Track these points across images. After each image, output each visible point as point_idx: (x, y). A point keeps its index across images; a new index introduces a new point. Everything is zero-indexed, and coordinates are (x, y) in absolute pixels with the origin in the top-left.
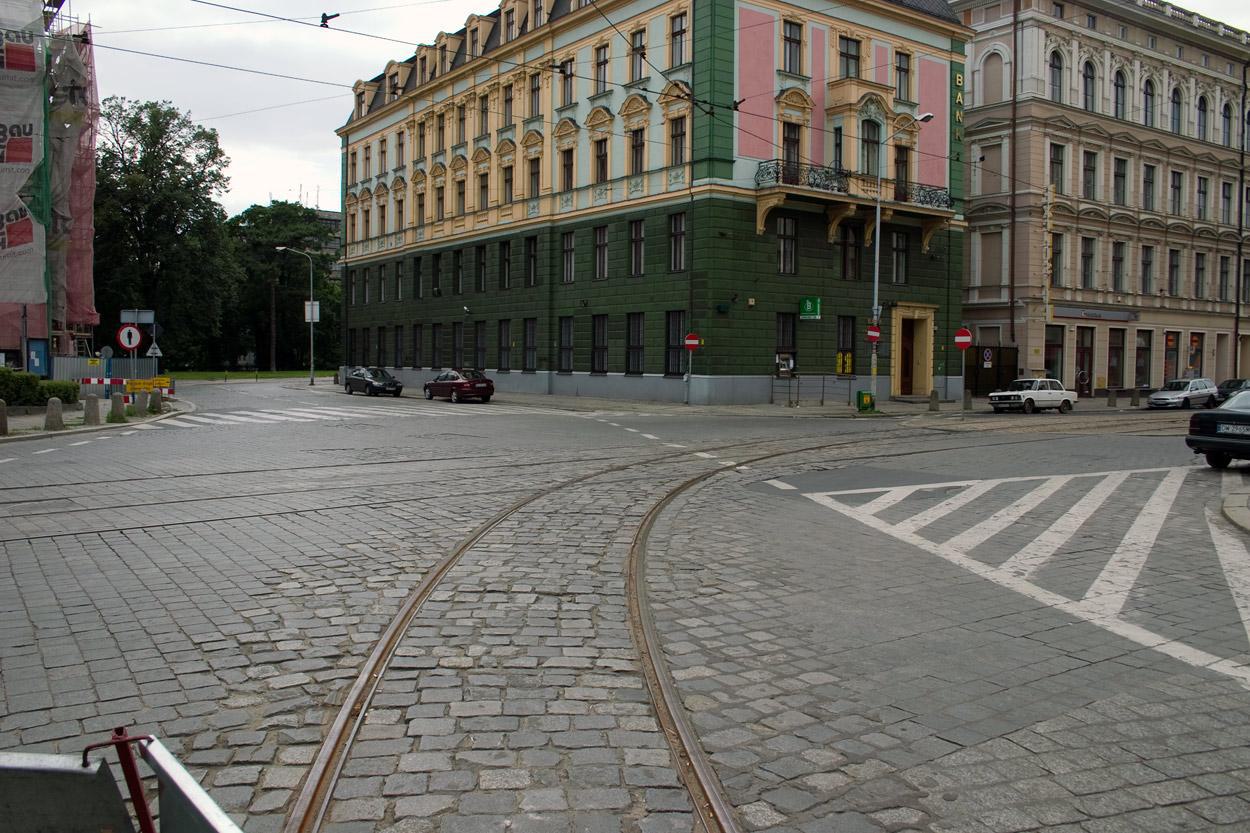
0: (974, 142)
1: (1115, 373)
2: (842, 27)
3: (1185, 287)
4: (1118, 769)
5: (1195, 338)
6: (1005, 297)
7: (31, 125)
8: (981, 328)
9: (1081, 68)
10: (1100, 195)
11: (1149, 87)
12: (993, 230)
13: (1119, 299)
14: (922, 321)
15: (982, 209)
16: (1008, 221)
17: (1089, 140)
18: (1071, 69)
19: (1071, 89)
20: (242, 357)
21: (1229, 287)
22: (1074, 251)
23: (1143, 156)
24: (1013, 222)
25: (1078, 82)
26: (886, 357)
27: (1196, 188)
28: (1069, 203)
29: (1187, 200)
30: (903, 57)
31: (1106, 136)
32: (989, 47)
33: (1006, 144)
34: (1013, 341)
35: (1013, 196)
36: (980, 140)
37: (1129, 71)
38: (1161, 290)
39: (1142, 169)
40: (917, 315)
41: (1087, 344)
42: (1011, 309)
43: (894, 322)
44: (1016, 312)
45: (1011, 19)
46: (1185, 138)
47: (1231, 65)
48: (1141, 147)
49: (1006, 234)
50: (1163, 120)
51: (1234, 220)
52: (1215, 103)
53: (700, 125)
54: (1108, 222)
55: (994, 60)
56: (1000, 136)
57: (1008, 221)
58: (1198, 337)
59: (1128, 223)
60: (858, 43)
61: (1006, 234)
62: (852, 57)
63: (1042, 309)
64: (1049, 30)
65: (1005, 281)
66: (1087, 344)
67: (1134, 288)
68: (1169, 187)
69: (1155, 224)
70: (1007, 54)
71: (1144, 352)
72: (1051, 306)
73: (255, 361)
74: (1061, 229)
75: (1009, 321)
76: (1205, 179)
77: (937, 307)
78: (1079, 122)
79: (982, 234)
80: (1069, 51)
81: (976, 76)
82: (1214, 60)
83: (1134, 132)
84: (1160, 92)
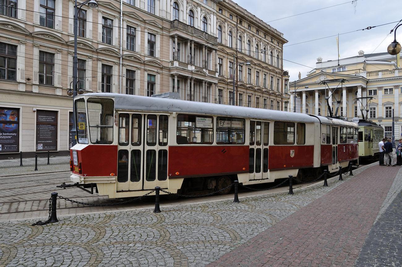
4: (361, 171)
5: (43, 118)
9: (202, 19)
18: (211, 25)
19: (159, 10)
23: (100, 11)
26: (43, 123)
27: (248, 72)
28: (159, 61)
29: (244, 76)
31: (226, 53)
39: (101, 21)
46: (274, 67)
48: (145, 23)
51: (280, 90)
52: (211, 21)
59: (157, 65)
64: (203, 8)
68: (228, 67)
73: (259, 125)
74: (242, 92)
76: (258, 72)
78: (256, 62)
80: (244, 36)
83: (275, 69)
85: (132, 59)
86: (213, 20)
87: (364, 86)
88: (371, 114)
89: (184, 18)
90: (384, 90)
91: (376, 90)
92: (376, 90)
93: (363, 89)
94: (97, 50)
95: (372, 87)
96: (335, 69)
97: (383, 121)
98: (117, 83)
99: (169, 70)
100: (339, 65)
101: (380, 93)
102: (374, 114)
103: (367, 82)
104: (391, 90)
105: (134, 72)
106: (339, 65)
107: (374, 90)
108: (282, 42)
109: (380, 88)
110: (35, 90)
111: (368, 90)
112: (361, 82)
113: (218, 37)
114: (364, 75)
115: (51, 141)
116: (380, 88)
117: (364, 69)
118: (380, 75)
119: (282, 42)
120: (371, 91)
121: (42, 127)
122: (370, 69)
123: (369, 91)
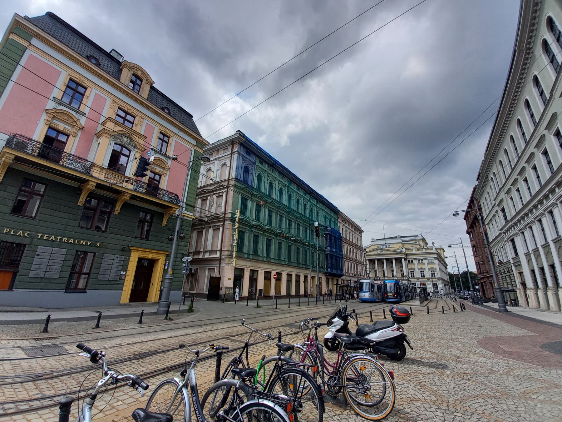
0: (214, 194)
2: (162, 129)
7: (119, 108)
10: (273, 225)
11: (298, 202)
20: (261, 96)
24: (224, 224)
25: (278, 193)
32: (223, 162)
33: (225, 194)
35: (225, 214)
42: (220, 260)
49: (221, 229)
53: (209, 361)
55: (225, 166)
60: (169, 137)
61: (221, 229)
62: (166, 142)
65: (219, 248)
67: (249, 251)
70: (228, 164)
71: (298, 282)
86: (321, 214)
93: (405, 259)
95: (410, 258)
99: (325, 251)
101: (415, 262)
103: (406, 255)
104: (422, 260)
108: (363, 232)
109: (415, 259)
114: (404, 250)
116: (415, 259)
117: (403, 246)
118: (414, 251)
119: (363, 232)
122: (407, 246)
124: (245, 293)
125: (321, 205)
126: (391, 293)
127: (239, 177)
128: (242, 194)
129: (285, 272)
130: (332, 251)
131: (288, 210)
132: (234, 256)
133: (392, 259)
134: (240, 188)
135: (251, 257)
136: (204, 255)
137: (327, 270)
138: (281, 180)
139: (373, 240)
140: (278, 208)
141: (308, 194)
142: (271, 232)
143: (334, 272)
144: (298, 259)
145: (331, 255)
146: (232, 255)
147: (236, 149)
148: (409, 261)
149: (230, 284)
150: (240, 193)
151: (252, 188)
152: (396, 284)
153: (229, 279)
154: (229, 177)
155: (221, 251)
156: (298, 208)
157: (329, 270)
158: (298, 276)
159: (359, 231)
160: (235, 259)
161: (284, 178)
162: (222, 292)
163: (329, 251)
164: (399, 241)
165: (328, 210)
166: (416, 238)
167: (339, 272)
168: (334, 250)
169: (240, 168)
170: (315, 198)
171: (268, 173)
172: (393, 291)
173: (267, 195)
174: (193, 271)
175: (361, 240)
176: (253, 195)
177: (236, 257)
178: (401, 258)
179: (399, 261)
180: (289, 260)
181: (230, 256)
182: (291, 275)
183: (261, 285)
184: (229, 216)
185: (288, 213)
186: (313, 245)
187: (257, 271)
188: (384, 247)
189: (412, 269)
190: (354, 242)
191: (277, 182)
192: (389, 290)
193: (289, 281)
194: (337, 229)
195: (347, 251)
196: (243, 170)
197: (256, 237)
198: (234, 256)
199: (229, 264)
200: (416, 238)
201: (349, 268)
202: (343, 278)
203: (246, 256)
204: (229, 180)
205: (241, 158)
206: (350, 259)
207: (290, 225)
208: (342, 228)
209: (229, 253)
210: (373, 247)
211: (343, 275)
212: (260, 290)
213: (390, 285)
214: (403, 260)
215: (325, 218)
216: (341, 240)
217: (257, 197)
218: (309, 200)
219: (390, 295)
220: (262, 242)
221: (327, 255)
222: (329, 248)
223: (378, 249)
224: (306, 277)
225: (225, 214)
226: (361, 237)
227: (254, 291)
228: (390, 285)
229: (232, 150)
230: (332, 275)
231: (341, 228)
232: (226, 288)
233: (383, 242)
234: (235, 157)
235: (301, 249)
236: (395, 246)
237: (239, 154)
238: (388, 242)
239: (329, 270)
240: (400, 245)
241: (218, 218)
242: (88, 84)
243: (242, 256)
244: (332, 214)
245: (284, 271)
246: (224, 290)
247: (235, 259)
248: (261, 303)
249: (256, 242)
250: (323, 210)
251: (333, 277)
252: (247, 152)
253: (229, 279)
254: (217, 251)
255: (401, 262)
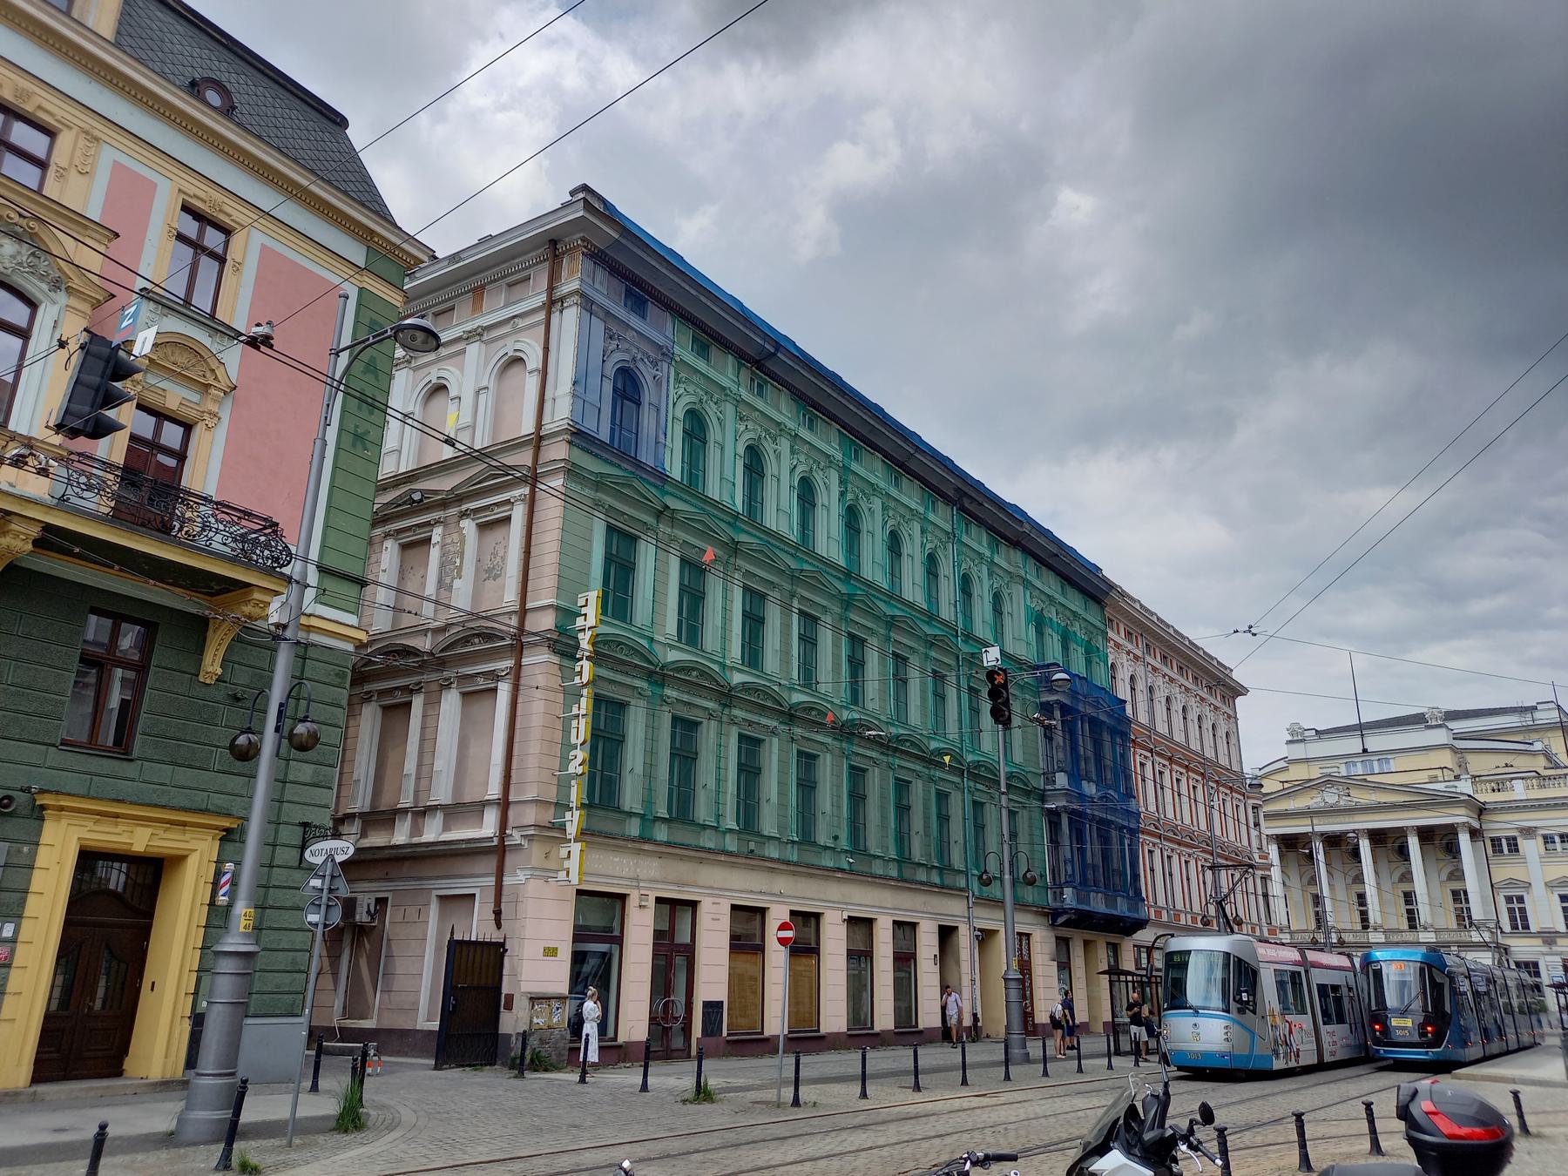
0: (464, 515)
1: (805, 995)
3: (878, 838)
6: (488, 827)
8: (441, 898)
12: (482, 684)
13: (752, 846)
14: (179, 860)
15: (466, 641)
16: (510, 663)
17: (752, 569)
21: (913, 833)
22: (783, 772)
24: (519, 666)
30: (205, 260)
32: (509, 348)
33: (518, 514)
34: (499, 926)
35: (523, 612)
36: (476, 511)
37: (649, 379)
38: (836, 838)
40: (140, 840)
41: (683, 937)
42: (499, 851)
43: (44, 857)
44: (510, 859)
45: (544, 297)
47: (740, 366)
49: (504, 689)
50: (912, 589)
51: (1245, 843)
54: (727, 696)
55: (515, 370)
56: (508, 502)
57: (510, 663)
58: (906, 929)
61: (504, 689)
63: (563, 853)
64: (1036, 593)
66: (683, 937)
67: (782, 827)
69: (703, 674)
70: (534, 360)
71: (905, 960)
72: (579, 845)
75: (491, 881)
77: (226, 823)
79: (464, 695)
81: (482, 398)
82: (1069, 590)
84: (719, 438)
85: (813, 715)
86: (1019, 604)
87: (1476, 824)
88: (1513, 919)
89: (1054, 652)
90: (1540, 840)
91: (1515, 839)
92: (1515, 839)
93: (1475, 834)
94: (662, 668)
95: (1501, 825)
96: (1355, 764)
97: (1560, 941)
98: (774, 798)
100: (1365, 751)
101: (1531, 848)
102: (1525, 918)
103: (1481, 810)
105: (622, 706)
106: (1365, 751)
107: (1507, 839)
108: (1236, 691)
109: (1529, 832)
110: (731, 844)
111: (1488, 835)
112: (1462, 811)
113: (1128, 698)
114: (1465, 787)
115: (98, 1005)
116: (1529, 832)
117: (1463, 765)
118: (1519, 791)
119: (1236, 691)
120: (1499, 839)
121: (79, 387)
123: (1492, 840)
124: (634, 1024)
125: (1017, 556)
126: (1404, 1013)
127: (589, 425)
128: (610, 511)
129: (837, 903)
130: (1082, 797)
131: (929, 630)
132: (572, 830)
133: (1401, 833)
134: (599, 483)
135: (661, 833)
136: (416, 830)
137: (1059, 895)
138: (804, 433)
139: (1298, 736)
140: (794, 577)
141: (948, 500)
142: (761, 699)
143: (1098, 904)
144: (902, 839)
145: (1077, 818)
146: (562, 828)
147: (569, 285)
148: (1496, 842)
149: (555, 976)
150: (598, 504)
151: (662, 477)
152: (1433, 971)
153: (551, 952)
154: (539, 425)
155: (504, 804)
156: (894, 574)
157: (1068, 893)
158: (906, 929)
159: (1228, 690)
160: (576, 848)
161: (819, 425)
162: (512, 1022)
163: (1067, 794)
164: (1440, 736)
165: (1050, 584)
166: (1527, 719)
167: (1122, 908)
168: (1090, 789)
169: (594, 381)
170: (981, 523)
171: (739, 402)
172: (1417, 1005)
173: (736, 516)
174: (361, 916)
175: (1232, 737)
176: (662, 513)
177: (585, 834)
178: (1451, 830)
179: (1440, 841)
180: (857, 846)
181: (553, 832)
182: (869, 922)
183: (713, 978)
184: (546, 622)
185: (847, 602)
186: (978, 765)
187: (693, 905)
188: (1359, 769)
189: (1512, 883)
190: (1209, 753)
191: (785, 445)
192: (1391, 1000)
193: (860, 956)
194: (1100, 677)
195: (1160, 796)
196: (608, 388)
197: (685, 728)
198: (572, 830)
199: (546, 874)
200: (1527, 719)
201: (1169, 882)
202: (1145, 936)
203: (634, 828)
204: (538, 440)
205: (598, 326)
206: (1180, 838)
207: (857, 665)
208: (1130, 677)
209: (548, 816)
210: (1298, 773)
211: (1141, 924)
212: (712, 1008)
213: (1398, 972)
214: (1464, 839)
215: (1039, 622)
216: (1124, 735)
217: (686, 525)
218: (951, 536)
219: (1404, 1026)
220: (645, 738)
221: (1053, 817)
222: (1062, 780)
223: (1328, 782)
224: (946, 934)
225: (523, 612)
226: (1232, 718)
227: (680, 1011)
228: (1398, 972)
229: (551, 289)
230: (1084, 920)
231: (1123, 674)
232: (534, 999)
233: (1352, 745)
234: (569, 321)
235: (918, 787)
236: (1418, 763)
237: (588, 304)
238: (1375, 742)
239: (1068, 893)
240: (1446, 759)
241: (488, 636)
242: (236, 215)
243: (615, 829)
244: (1075, 602)
245: (717, 891)
246: (521, 1005)
247: (576, 848)
248: (718, 1074)
249: (685, 758)
250: (1027, 584)
251: (1089, 935)
252: (629, 293)
253: (551, 952)
254: (484, 804)
255: (1453, 850)
